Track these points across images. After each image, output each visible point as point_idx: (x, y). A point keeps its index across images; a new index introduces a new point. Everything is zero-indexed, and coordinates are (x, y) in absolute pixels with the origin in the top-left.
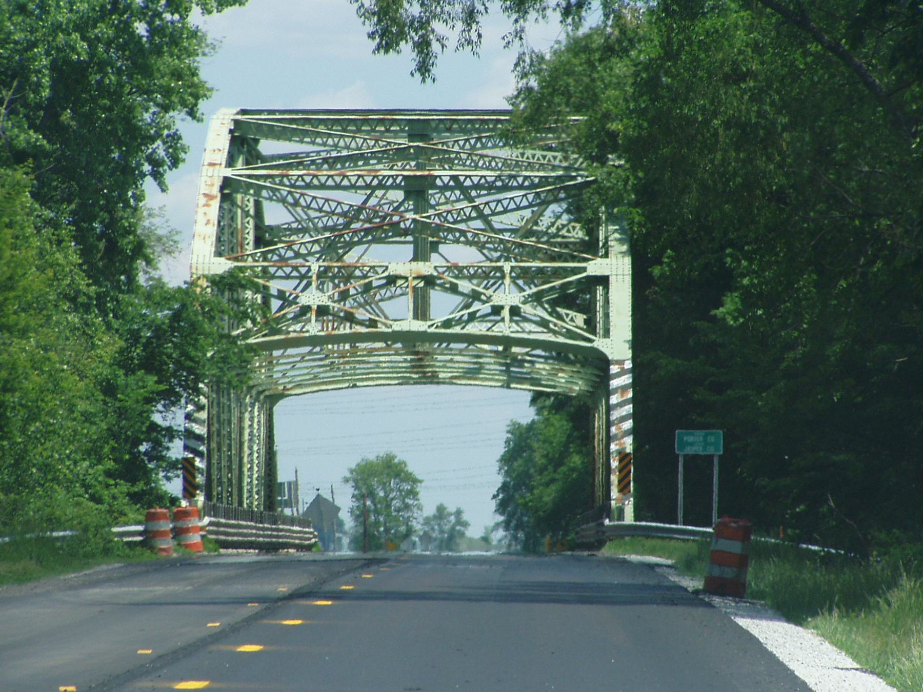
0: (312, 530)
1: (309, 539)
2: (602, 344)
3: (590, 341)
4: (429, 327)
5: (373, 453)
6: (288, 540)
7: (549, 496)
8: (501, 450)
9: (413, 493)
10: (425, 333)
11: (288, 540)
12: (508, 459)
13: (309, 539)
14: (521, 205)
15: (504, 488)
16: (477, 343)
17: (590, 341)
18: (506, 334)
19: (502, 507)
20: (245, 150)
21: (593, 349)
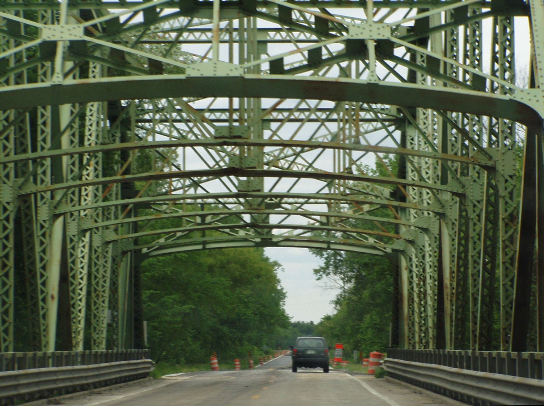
0: (150, 360)
1: (149, 368)
13: (149, 368)
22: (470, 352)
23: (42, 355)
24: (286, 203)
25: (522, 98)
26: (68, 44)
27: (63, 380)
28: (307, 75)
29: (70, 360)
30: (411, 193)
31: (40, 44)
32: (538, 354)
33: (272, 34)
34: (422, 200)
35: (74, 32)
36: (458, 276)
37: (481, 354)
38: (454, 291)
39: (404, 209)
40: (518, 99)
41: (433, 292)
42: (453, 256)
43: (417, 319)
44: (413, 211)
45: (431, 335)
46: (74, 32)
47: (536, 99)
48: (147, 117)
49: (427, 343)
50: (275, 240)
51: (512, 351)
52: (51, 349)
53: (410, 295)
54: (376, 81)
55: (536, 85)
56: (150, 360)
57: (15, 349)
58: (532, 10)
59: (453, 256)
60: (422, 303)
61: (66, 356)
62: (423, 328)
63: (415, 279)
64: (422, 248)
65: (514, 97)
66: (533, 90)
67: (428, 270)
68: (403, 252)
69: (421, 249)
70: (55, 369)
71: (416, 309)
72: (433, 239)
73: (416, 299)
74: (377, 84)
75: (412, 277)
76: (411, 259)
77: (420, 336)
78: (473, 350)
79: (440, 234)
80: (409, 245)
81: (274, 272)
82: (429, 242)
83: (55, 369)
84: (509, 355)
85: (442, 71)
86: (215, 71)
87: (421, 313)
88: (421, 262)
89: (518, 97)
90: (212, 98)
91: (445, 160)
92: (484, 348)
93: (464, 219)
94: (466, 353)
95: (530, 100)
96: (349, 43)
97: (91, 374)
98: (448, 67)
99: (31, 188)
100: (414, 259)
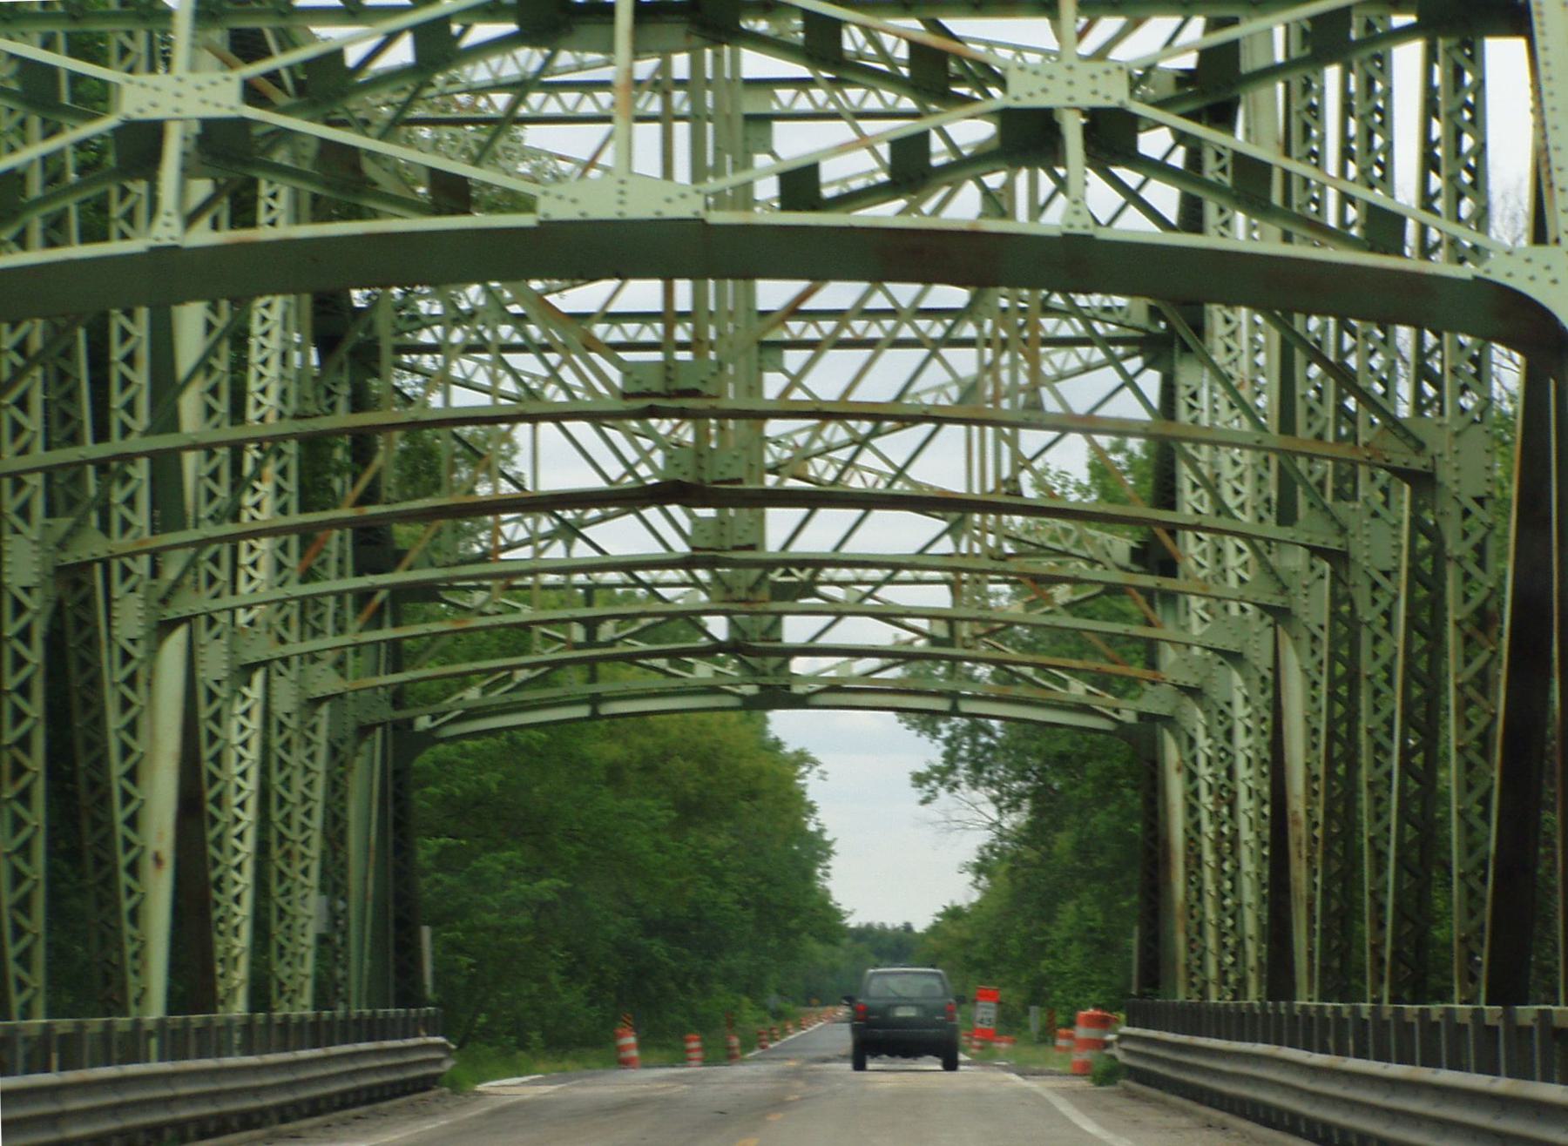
0: (440, 1040)
1: (438, 1062)
2: (1529, 270)
10: (699, 224)
13: (438, 1062)
22: (1366, 1007)
24: (831, 582)
25: (1509, 275)
26: (196, 128)
27: (192, 1099)
28: (887, 212)
29: (211, 1041)
30: (1192, 549)
31: (116, 131)
33: (785, 95)
35: (211, 94)
36: (1329, 789)
37: (1398, 1013)
38: (1318, 832)
39: (1170, 598)
40: (1498, 276)
41: (1258, 834)
42: (1315, 732)
43: (1211, 915)
44: (1196, 603)
45: (1252, 961)
46: (211, 94)
47: (1550, 275)
48: (426, 337)
49: (1242, 982)
50: (798, 689)
52: (156, 1008)
53: (1192, 844)
55: (1551, 236)
56: (440, 1040)
58: (1535, 19)
59: (1315, 732)
60: (1227, 866)
61: (198, 1031)
64: (1225, 708)
65: (1488, 271)
66: (1540, 249)
67: (1242, 772)
68: (1169, 721)
70: (167, 1066)
71: (1210, 886)
72: (1257, 684)
73: (1209, 857)
77: (1220, 964)
78: (1374, 1001)
79: (1276, 669)
80: (1188, 701)
83: (167, 1066)
85: (1276, 198)
88: (1222, 749)
89: (1497, 270)
90: (615, 283)
91: (1288, 455)
92: (1405, 995)
93: (1345, 625)
95: (1532, 278)
96: (1008, 118)
97: (270, 1080)
98: (1296, 185)
99: (92, 545)
100: (1203, 742)
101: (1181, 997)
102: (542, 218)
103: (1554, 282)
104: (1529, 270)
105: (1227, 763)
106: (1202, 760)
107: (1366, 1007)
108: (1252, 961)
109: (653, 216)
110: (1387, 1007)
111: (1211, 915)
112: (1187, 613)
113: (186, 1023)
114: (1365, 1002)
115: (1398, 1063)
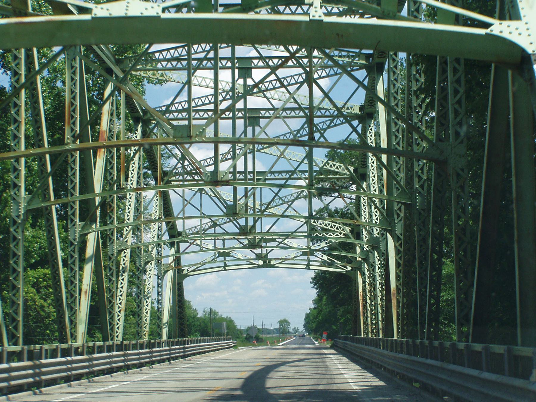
0: (232, 341)
1: (231, 345)
2: (509, 30)
3: (487, 25)
4: (164, 10)
5: (282, 318)
6: (195, 352)
7: (314, 325)
8: (304, 317)
9: (289, 325)
10: (157, 18)
11: (195, 352)
12: (305, 319)
13: (231, 345)
14: (322, 76)
15: (305, 324)
16: (257, 44)
17: (487, 25)
18: (317, 18)
19: (304, 327)
20: (114, 78)
21: (488, 36)
22: (418, 341)
23: (55, 348)
25: (501, 32)
27: (179, 353)
32: (526, 351)
33: (263, 112)
34: (372, 220)
41: (382, 294)
43: (369, 315)
45: (380, 327)
47: (518, 32)
49: (378, 332)
50: (272, 263)
51: (472, 342)
53: (364, 290)
54: (320, 16)
56: (232, 341)
57: (25, 344)
60: (373, 303)
61: (172, 342)
62: (374, 322)
63: (368, 294)
64: (373, 264)
65: (492, 31)
67: (378, 278)
69: (372, 265)
70: (63, 359)
71: (369, 308)
73: (368, 301)
74: (322, 20)
75: (365, 286)
76: (364, 274)
77: (372, 328)
78: (421, 339)
81: (263, 281)
82: (379, 258)
83: (63, 359)
84: (467, 347)
86: (127, 10)
87: (373, 311)
88: (372, 274)
94: (414, 342)
95: (510, 33)
97: (165, 353)
100: (367, 273)
101: (362, 336)
102: (93, 16)
103: (520, 34)
104: (509, 30)
105: (373, 277)
106: (367, 277)
107: (418, 341)
108: (380, 327)
109: (139, 15)
110: (426, 342)
111: (369, 315)
112: (363, 235)
113: (170, 340)
114: (418, 339)
115: (430, 359)
